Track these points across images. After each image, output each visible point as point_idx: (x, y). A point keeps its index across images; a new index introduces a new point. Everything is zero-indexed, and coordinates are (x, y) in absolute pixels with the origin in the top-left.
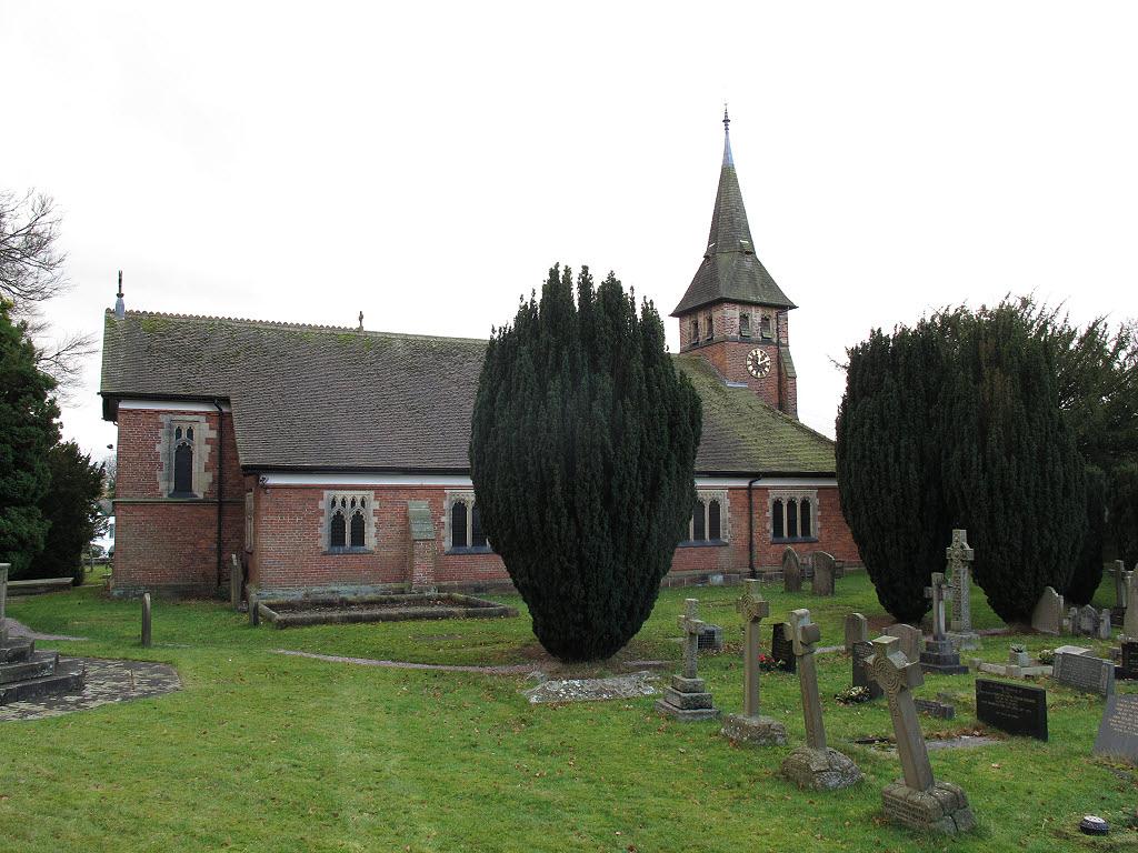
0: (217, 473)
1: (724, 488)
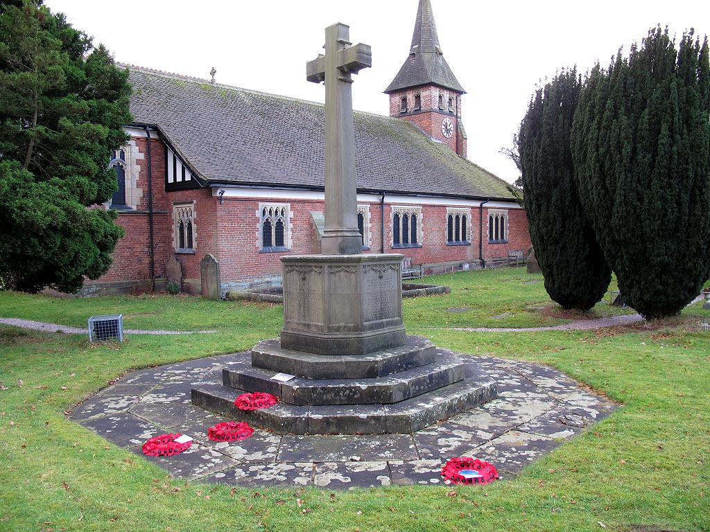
0: (147, 189)
1: (469, 207)
